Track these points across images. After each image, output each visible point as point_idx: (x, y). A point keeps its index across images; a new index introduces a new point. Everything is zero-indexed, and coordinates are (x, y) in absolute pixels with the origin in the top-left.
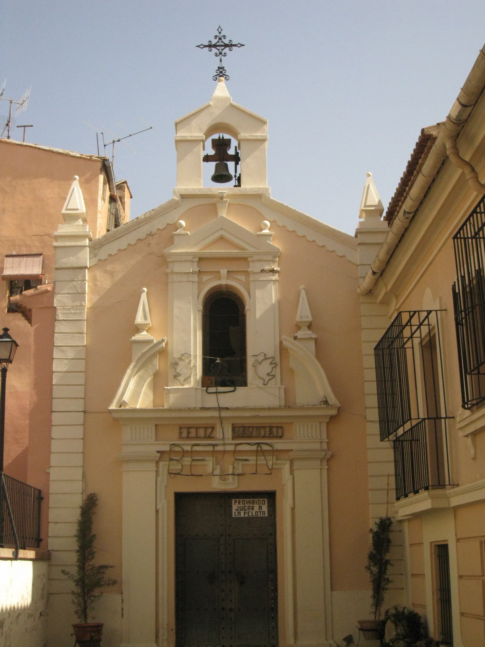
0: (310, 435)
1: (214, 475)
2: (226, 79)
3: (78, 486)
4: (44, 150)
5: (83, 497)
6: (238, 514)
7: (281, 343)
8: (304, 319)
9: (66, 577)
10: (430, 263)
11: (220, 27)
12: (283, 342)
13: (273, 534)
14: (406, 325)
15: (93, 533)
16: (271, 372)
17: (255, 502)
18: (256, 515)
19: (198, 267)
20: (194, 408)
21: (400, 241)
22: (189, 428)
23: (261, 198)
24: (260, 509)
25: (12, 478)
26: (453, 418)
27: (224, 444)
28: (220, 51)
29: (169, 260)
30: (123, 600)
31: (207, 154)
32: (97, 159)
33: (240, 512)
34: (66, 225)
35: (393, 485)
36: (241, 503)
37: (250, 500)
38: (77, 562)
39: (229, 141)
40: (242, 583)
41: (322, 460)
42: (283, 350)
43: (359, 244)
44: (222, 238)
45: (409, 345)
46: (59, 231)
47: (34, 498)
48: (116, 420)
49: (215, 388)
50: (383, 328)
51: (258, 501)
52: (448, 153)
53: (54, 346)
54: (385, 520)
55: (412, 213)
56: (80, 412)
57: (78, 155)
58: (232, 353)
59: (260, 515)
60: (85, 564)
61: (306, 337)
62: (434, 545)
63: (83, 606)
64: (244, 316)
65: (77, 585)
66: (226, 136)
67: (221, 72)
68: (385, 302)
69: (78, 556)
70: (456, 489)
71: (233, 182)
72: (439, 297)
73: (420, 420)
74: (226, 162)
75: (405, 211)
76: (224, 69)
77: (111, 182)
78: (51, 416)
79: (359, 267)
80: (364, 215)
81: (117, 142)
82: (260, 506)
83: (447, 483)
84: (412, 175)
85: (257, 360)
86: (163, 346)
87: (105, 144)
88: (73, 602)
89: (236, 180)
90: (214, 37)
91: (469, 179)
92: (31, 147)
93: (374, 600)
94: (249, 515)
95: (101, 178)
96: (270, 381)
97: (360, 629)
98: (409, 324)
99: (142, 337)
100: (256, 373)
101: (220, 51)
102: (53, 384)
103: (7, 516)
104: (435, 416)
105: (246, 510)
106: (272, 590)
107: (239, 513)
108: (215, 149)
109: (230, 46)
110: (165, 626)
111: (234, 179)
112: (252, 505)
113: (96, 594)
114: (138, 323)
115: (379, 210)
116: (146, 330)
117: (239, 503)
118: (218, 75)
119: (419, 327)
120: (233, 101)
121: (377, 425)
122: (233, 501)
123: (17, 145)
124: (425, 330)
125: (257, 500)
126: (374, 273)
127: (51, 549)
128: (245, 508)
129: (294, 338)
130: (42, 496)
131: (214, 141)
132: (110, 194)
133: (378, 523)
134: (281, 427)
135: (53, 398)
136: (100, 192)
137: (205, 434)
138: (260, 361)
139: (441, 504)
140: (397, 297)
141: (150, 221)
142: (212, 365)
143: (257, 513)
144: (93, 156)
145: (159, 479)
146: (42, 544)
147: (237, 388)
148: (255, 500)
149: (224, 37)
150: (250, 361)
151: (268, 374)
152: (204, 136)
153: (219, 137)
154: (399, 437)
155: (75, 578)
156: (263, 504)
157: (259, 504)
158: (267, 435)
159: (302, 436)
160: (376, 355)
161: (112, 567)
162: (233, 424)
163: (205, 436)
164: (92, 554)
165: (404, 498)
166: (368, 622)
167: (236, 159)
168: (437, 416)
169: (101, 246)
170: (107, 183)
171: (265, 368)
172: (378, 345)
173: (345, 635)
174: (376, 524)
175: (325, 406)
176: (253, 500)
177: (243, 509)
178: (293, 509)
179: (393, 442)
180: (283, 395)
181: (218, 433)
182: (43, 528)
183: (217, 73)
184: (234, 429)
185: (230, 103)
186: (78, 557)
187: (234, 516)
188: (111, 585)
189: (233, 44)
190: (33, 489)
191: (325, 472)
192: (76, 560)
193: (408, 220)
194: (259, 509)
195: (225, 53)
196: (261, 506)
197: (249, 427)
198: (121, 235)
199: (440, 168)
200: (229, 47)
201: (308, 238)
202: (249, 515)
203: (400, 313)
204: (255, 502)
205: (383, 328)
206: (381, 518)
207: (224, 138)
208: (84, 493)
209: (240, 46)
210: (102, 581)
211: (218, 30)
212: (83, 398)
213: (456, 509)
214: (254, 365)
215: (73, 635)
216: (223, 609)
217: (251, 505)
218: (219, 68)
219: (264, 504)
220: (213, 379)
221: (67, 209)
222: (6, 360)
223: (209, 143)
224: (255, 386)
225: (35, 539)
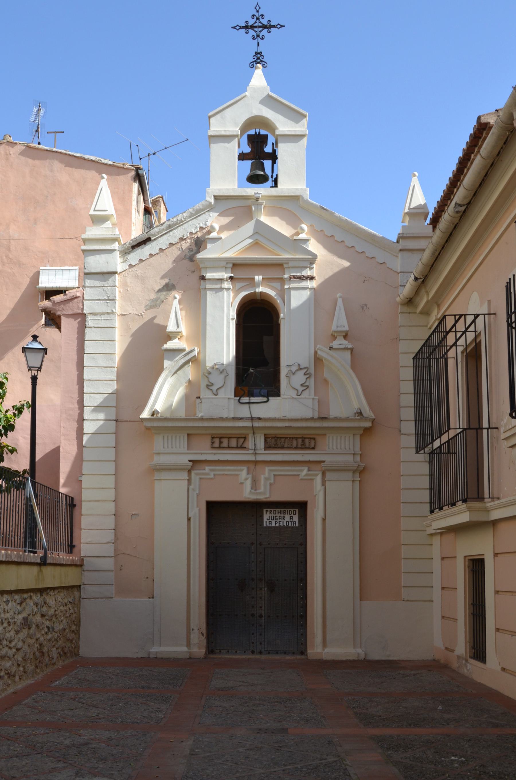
0: (343, 447)
2: (264, 66)
4: (75, 156)
6: (269, 524)
7: (316, 353)
8: (340, 329)
10: (491, 248)
11: (257, 4)
12: (318, 353)
13: (304, 544)
14: (450, 331)
17: (286, 513)
18: (287, 525)
20: (227, 418)
21: (447, 241)
22: (221, 438)
23: (299, 199)
24: (291, 519)
26: (497, 428)
28: (258, 34)
29: (201, 265)
31: (242, 152)
32: (131, 167)
33: (271, 522)
34: (94, 227)
36: (272, 513)
37: (281, 510)
39: (266, 137)
41: (354, 472)
42: (318, 360)
43: (401, 250)
45: (451, 353)
46: (87, 233)
47: (66, 504)
48: (148, 429)
49: (248, 398)
50: (413, 353)
51: (290, 511)
53: (84, 354)
55: (464, 205)
56: (112, 420)
57: (110, 163)
58: (264, 363)
59: (291, 525)
61: (341, 347)
62: (468, 559)
66: (263, 132)
67: (258, 58)
68: (426, 312)
70: (497, 502)
71: (270, 182)
72: (488, 301)
74: (262, 161)
75: (456, 203)
76: (262, 54)
77: (145, 192)
79: (400, 274)
80: (407, 219)
81: (152, 155)
82: (290, 517)
83: (486, 495)
84: (462, 174)
85: (290, 370)
86: (196, 355)
87: (141, 158)
89: (273, 181)
90: (251, 16)
92: (61, 153)
94: (280, 524)
95: (135, 186)
96: (304, 392)
98: (454, 330)
99: (174, 345)
100: (290, 384)
101: (258, 33)
102: (84, 392)
104: (478, 427)
105: (277, 520)
106: (302, 598)
107: (270, 523)
108: (251, 146)
109: (268, 27)
111: (270, 179)
112: (283, 515)
114: (170, 331)
115: (424, 213)
116: (179, 339)
117: (270, 513)
118: (255, 61)
119: (467, 329)
120: (270, 91)
121: (413, 438)
122: (265, 510)
123: (47, 150)
124: (470, 336)
125: (289, 510)
126: (416, 279)
128: (276, 517)
130: (74, 503)
131: (250, 137)
132: (145, 206)
134: (314, 439)
135: (84, 407)
136: (134, 203)
137: (237, 444)
138: (294, 372)
139: (481, 517)
140: (439, 306)
142: (245, 375)
143: (287, 523)
144: (126, 164)
145: (191, 487)
146: (75, 550)
147: (270, 398)
148: (286, 510)
149: (262, 17)
150: (284, 372)
152: (239, 131)
153: (256, 133)
154: (436, 449)
156: (294, 514)
157: (290, 514)
158: (299, 446)
159: (334, 447)
160: (416, 367)
162: (265, 435)
163: (237, 446)
165: (439, 510)
170: (141, 194)
171: (299, 378)
172: (415, 356)
175: (359, 418)
176: (284, 511)
177: (274, 518)
178: (324, 520)
179: (428, 455)
180: (316, 408)
181: (250, 444)
182: (75, 535)
183: (254, 59)
184: (266, 439)
185: (267, 93)
187: (265, 525)
189: (272, 25)
190: (64, 496)
191: (357, 484)
193: (459, 215)
194: (290, 519)
195: (263, 36)
196: (292, 516)
197: (281, 438)
199: (502, 148)
200: (268, 28)
201: (347, 244)
202: (280, 524)
203: (444, 317)
204: (286, 513)
207: (261, 134)
209: (280, 28)
211: (255, 8)
212: (115, 407)
213: (494, 523)
214: (287, 376)
216: (253, 615)
217: (282, 515)
218: (257, 53)
219: (296, 514)
220: (246, 389)
221: (95, 210)
223: (245, 140)
224: (290, 397)
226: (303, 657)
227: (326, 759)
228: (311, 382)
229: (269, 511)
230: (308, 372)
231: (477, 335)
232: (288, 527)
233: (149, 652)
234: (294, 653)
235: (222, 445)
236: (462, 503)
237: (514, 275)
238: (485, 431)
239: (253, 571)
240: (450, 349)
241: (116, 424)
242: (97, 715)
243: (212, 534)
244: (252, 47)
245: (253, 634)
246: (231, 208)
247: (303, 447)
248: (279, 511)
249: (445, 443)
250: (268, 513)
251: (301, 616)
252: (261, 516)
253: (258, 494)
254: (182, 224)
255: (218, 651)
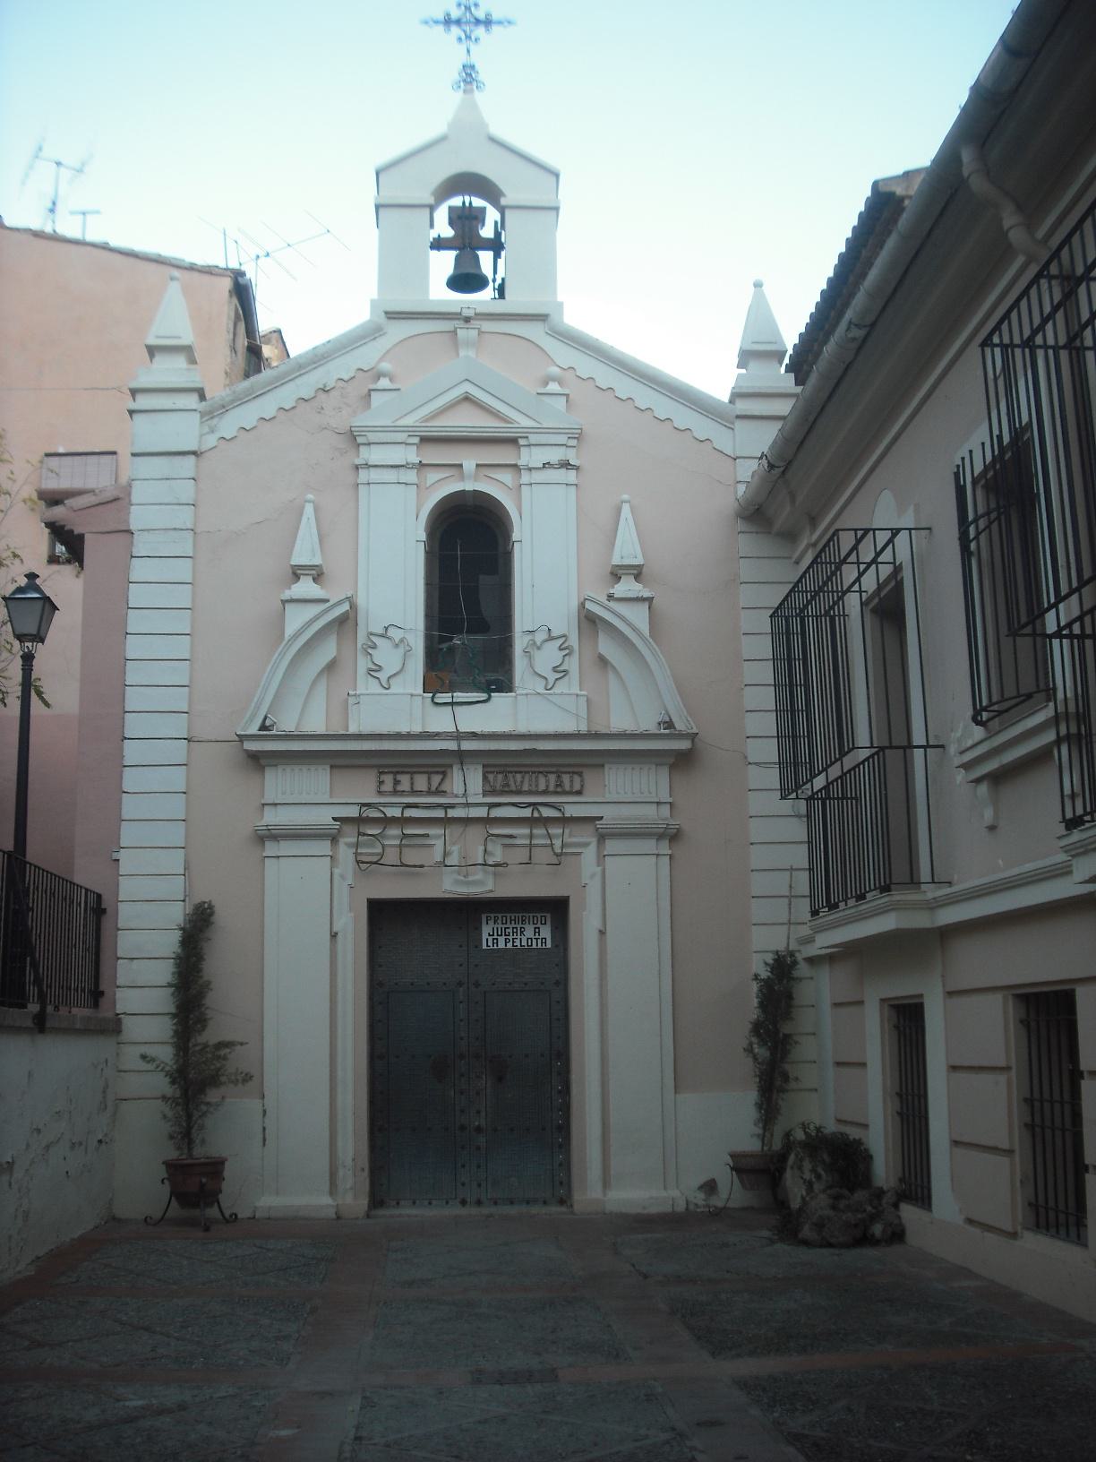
1: (446, 866)
3: (176, 887)
5: (185, 908)
6: (493, 943)
9: (150, 1067)
13: (563, 982)
15: (205, 978)
16: (560, 665)
17: (527, 921)
19: (417, 456)
25: (35, 866)
26: (942, 746)
27: (468, 805)
30: (265, 1112)
35: (804, 888)
36: (499, 921)
37: (517, 915)
38: (173, 1037)
39: (483, 210)
40: (500, 1079)
44: (467, 398)
50: (790, 583)
52: (965, 173)
54: (784, 956)
60: (188, 1040)
63: (184, 1124)
64: (508, 556)
65: (173, 1082)
66: (478, 202)
69: (174, 1024)
73: (874, 750)
75: (850, 322)
78: (121, 749)
82: (535, 928)
83: (925, 874)
88: (165, 1116)
91: (1011, 228)
93: (760, 1112)
97: (732, 1169)
103: (38, 946)
106: (560, 1092)
107: (495, 941)
110: (349, 1162)
113: (214, 1100)
122: (484, 917)
124: (885, 571)
127: (122, 1012)
129: (609, 596)
130: (103, 907)
131: (451, 209)
133: (771, 962)
141: (322, 362)
146: (104, 1002)
148: (527, 915)
150: (519, 643)
151: (555, 669)
153: (464, 203)
155: (168, 1068)
158: (552, 788)
161: (242, 1044)
164: (203, 1022)
166: (752, 1155)
167: (496, 246)
168: (905, 751)
169: (224, 410)
171: (548, 657)
172: (774, 613)
173: (703, 1179)
174: (766, 964)
178: (602, 933)
186: (174, 1027)
187: (484, 947)
188: (240, 1085)
190: (83, 891)
192: (171, 1033)
198: (262, 392)
204: (527, 921)
205: (790, 583)
206: (777, 952)
208: (187, 901)
210: (223, 1075)
215: (165, 1181)
216: (463, 1128)
222: (31, 635)
223: (442, 215)
225: (90, 991)
226: (563, 1209)
227: (647, 1437)
228: (573, 664)
229: (493, 918)
230: (566, 645)
231: (898, 569)
232: (530, 949)
233: (255, 1207)
234: (545, 1203)
235: (399, 788)
236: (857, 901)
237: (971, 452)
238: (918, 753)
239: (462, 1039)
240: (865, 570)
241: (189, 746)
242: (152, 1351)
243: (380, 966)
244: (457, 56)
245: (463, 1166)
246: (415, 335)
247: (559, 789)
248: (513, 918)
249: (836, 780)
250: (491, 922)
251: (560, 1128)
252: (476, 929)
253: (469, 883)
254: (322, 362)
255: (394, 1203)
